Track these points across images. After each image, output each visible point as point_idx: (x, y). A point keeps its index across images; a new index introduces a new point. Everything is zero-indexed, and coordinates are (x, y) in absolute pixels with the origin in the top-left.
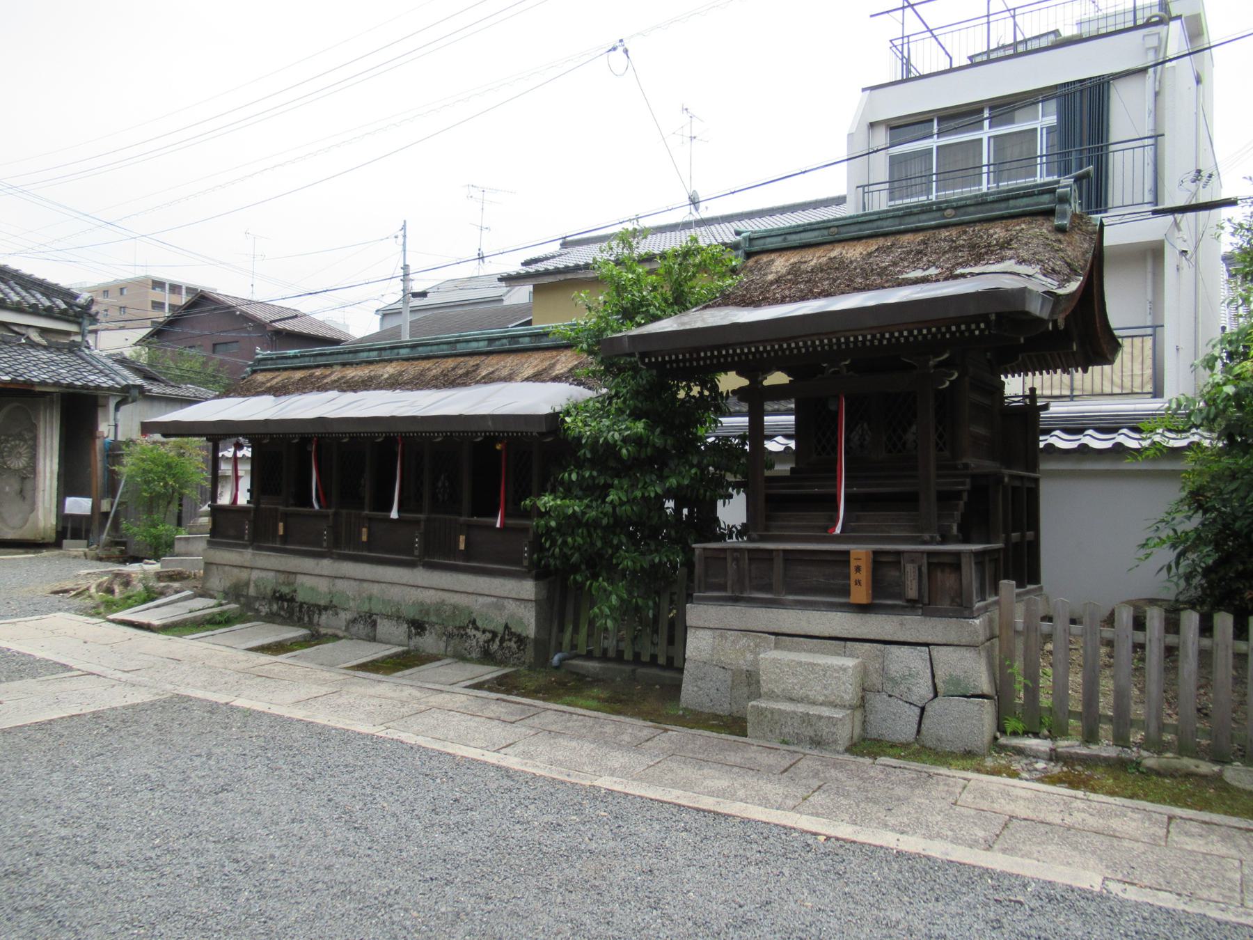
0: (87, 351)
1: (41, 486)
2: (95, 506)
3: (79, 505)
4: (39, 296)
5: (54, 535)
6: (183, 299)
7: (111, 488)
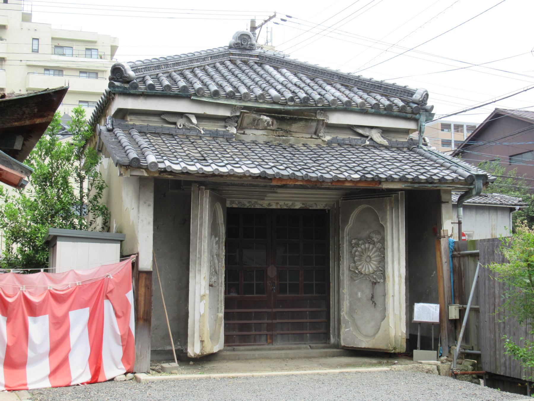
0: (425, 148)
1: (390, 292)
2: (443, 313)
3: (427, 312)
4: (379, 97)
5: (404, 345)
6: (464, 136)
7: (459, 294)
